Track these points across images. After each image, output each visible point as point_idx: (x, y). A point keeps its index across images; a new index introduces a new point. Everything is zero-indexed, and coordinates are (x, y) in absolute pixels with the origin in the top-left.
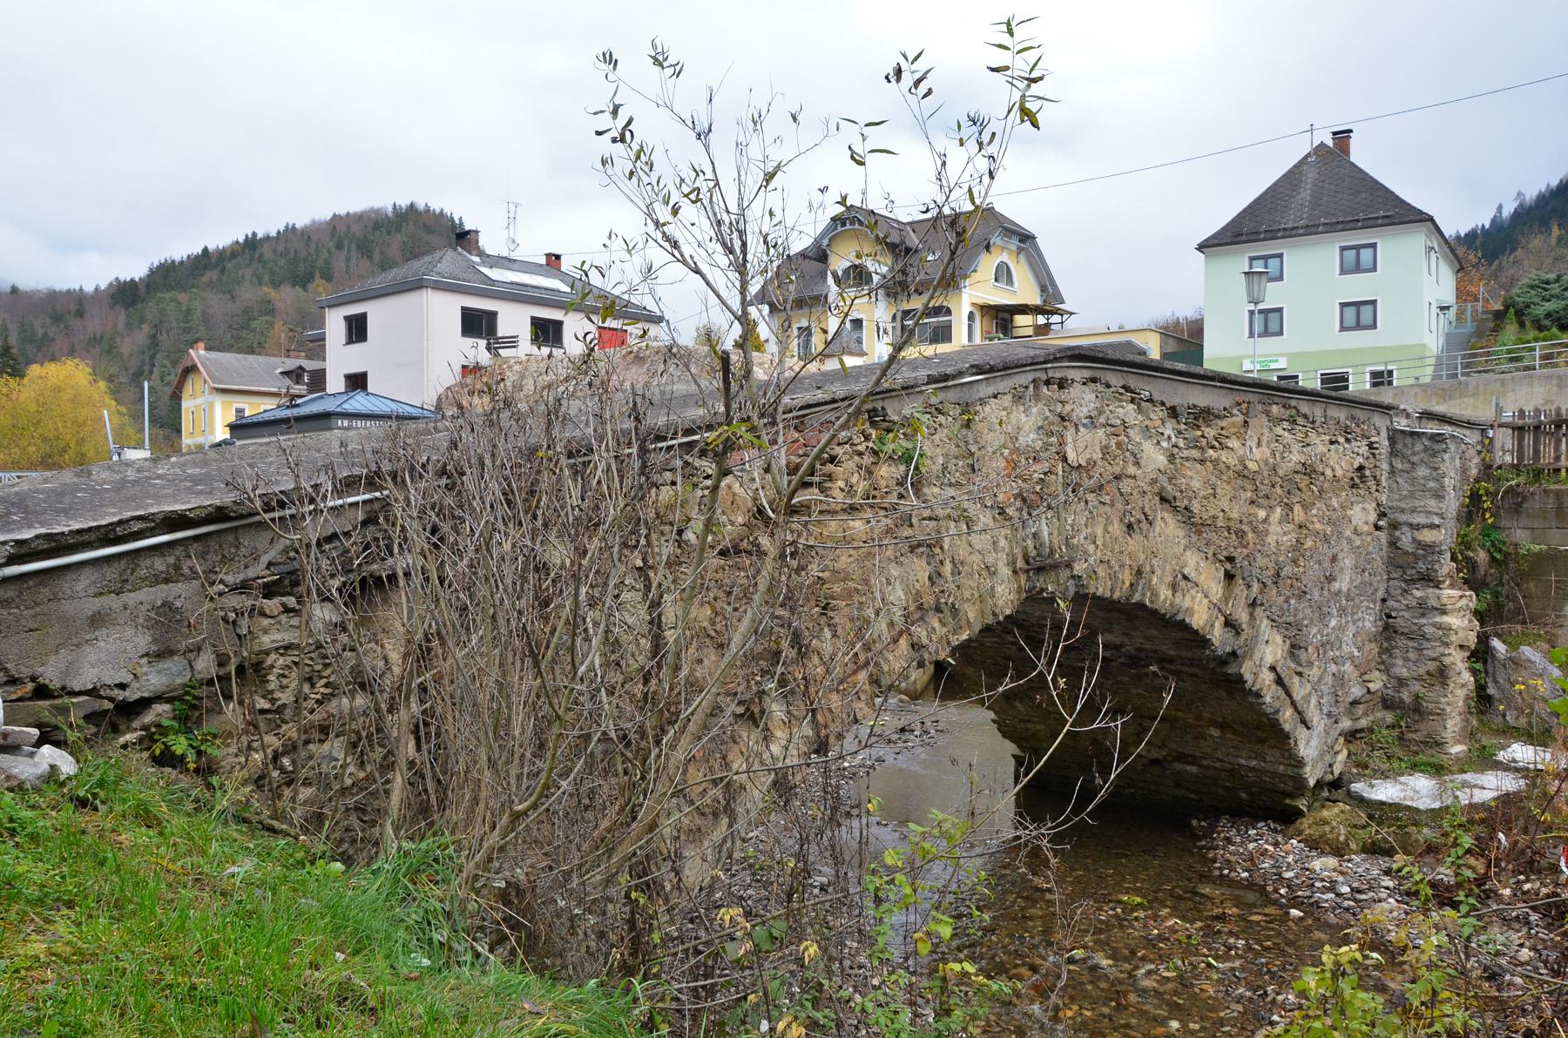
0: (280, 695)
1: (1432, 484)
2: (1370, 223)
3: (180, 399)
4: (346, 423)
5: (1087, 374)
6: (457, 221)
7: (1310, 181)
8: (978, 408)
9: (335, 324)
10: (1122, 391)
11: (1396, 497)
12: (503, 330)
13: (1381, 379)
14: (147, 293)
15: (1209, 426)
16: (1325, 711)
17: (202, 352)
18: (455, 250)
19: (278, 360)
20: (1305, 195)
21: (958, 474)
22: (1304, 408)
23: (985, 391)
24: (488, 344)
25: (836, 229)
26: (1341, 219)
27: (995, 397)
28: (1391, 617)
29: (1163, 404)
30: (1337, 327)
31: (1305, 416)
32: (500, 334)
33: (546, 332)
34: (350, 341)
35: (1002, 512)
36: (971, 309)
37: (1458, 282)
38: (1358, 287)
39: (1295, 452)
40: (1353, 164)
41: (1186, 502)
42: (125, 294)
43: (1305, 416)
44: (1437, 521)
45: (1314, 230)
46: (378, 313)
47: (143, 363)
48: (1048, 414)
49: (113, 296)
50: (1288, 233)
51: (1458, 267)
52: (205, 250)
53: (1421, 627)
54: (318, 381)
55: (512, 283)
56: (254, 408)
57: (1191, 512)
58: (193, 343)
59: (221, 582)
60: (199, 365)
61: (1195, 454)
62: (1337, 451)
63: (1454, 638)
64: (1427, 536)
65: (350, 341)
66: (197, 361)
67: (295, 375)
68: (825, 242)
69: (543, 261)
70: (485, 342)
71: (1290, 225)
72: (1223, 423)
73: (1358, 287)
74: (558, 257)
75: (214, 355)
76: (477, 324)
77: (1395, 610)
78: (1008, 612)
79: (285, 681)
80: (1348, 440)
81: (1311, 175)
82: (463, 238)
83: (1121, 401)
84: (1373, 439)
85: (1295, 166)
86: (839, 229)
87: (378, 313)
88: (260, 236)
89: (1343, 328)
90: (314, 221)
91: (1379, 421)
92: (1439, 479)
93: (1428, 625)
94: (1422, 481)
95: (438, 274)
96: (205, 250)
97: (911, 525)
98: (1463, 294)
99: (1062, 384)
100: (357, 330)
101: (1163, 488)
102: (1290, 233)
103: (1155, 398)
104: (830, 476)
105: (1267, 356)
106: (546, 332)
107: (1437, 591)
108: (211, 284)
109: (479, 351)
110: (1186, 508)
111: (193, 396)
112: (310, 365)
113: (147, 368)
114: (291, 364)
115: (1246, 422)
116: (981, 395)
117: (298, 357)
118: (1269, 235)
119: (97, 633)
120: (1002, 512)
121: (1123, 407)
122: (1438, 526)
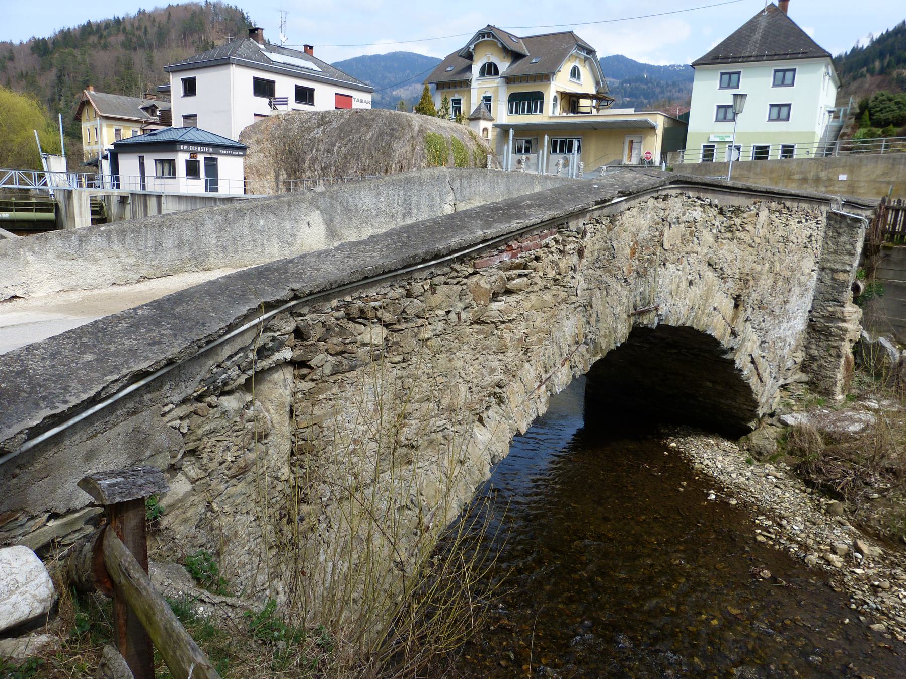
0: (210, 465)
1: (848, 247)
2: (795, 56)
3: (80, 121)
4: (185, 148)
5: (679, 191)
6: (245, 15)
7: (762, 27)
8: (619, 218)
9: (176, 84)
10: (696, 200)
11: (826, 252)
12: (278, 93)
13: (788, 151)
14: (54, 48)
15: (737, 217)
16: (773, 376)
17: (92, 92)
18: (249, 40)
19: (140, 100)
20: (758, 36)
21: (604, 261)
22: (788, 204)
23: (625, 206)
24: (270, 102)
25: (479, 39)
26: (778, 53)
27: (628, 209)
28: (813, 321)
29: (716, 206)
30: (767, 119)
31: (788, 208)
32: (276, 96)
33: (304, 95)
34: (186, 95)
35: (626, 281)
36: (555, 94)
37: (838, 93)
38: (782, 95)
39: (780, 230)
40: (789, 18)
41: (721, 265)
42: (40, 47)
43: (788, 208)
44: (848, 268)
45: (761, 58)
46: (202, 79)
47: (54, 93)
48: (656, 218)
49: (33, 49)
50: (745, 59)
51: (839, 84)
52: (89, 22)
53: (829, 328)
54: (166, 117)
55: (284, 64)
56: (127, 134)
57: (723, 271)
58: (87, 86)
59: (171, 402)
60: (91, 101)
61: (729, 235)
62: (800, 228)
63: (847, 336)
64: (841, 277)
65: (186, 95)
66: (89, 98)
67: (151, 109)
68: (472, 47)
69: (302, 49)
70: (267, 100)
71: (747, 54)
72: (745, 215)
73: (782, 95)
74: (311, 48)
75: (101, 95)
76: (263, 88)
77: (815, 317)
78: (623, 341)
79: (212, 455)
80: (807, 220)
81: (763, 23)
82: (254, 32)
83: (694, 206)
84: (819, 219)
85: (755, 18)
86: (481, 40)
87: (202, 79)
88: (121, 18)
89: (770, 120)
90: (156, 8)
91: (824, 209)
92: (853, 245)
93: (833, 327)
94: (843, 244)
95: (240, 56)
96: (89, 22)
97: (577, 295)
98: (840, 99)
99: (665, 198)
100: (190, 88)
101: (710, 258)
102: (747, 59)
103: (713, 203)
104: (534, 269)
105: (725, 133)
106: (304, 95)
107: (842, 309)
108: (94, 46)
109: (262, 104)
110: (721, 269)
111: (88, 120)
112: (161, 105)
113: (57, 97)
114: (148, 103)
115: (757, 214)
116: (622, 209)
117: (152, 99)
118: (734, 60)
119: (90, 465)
120: (626, 281)
121: (696, 210)
122: (848, 271)
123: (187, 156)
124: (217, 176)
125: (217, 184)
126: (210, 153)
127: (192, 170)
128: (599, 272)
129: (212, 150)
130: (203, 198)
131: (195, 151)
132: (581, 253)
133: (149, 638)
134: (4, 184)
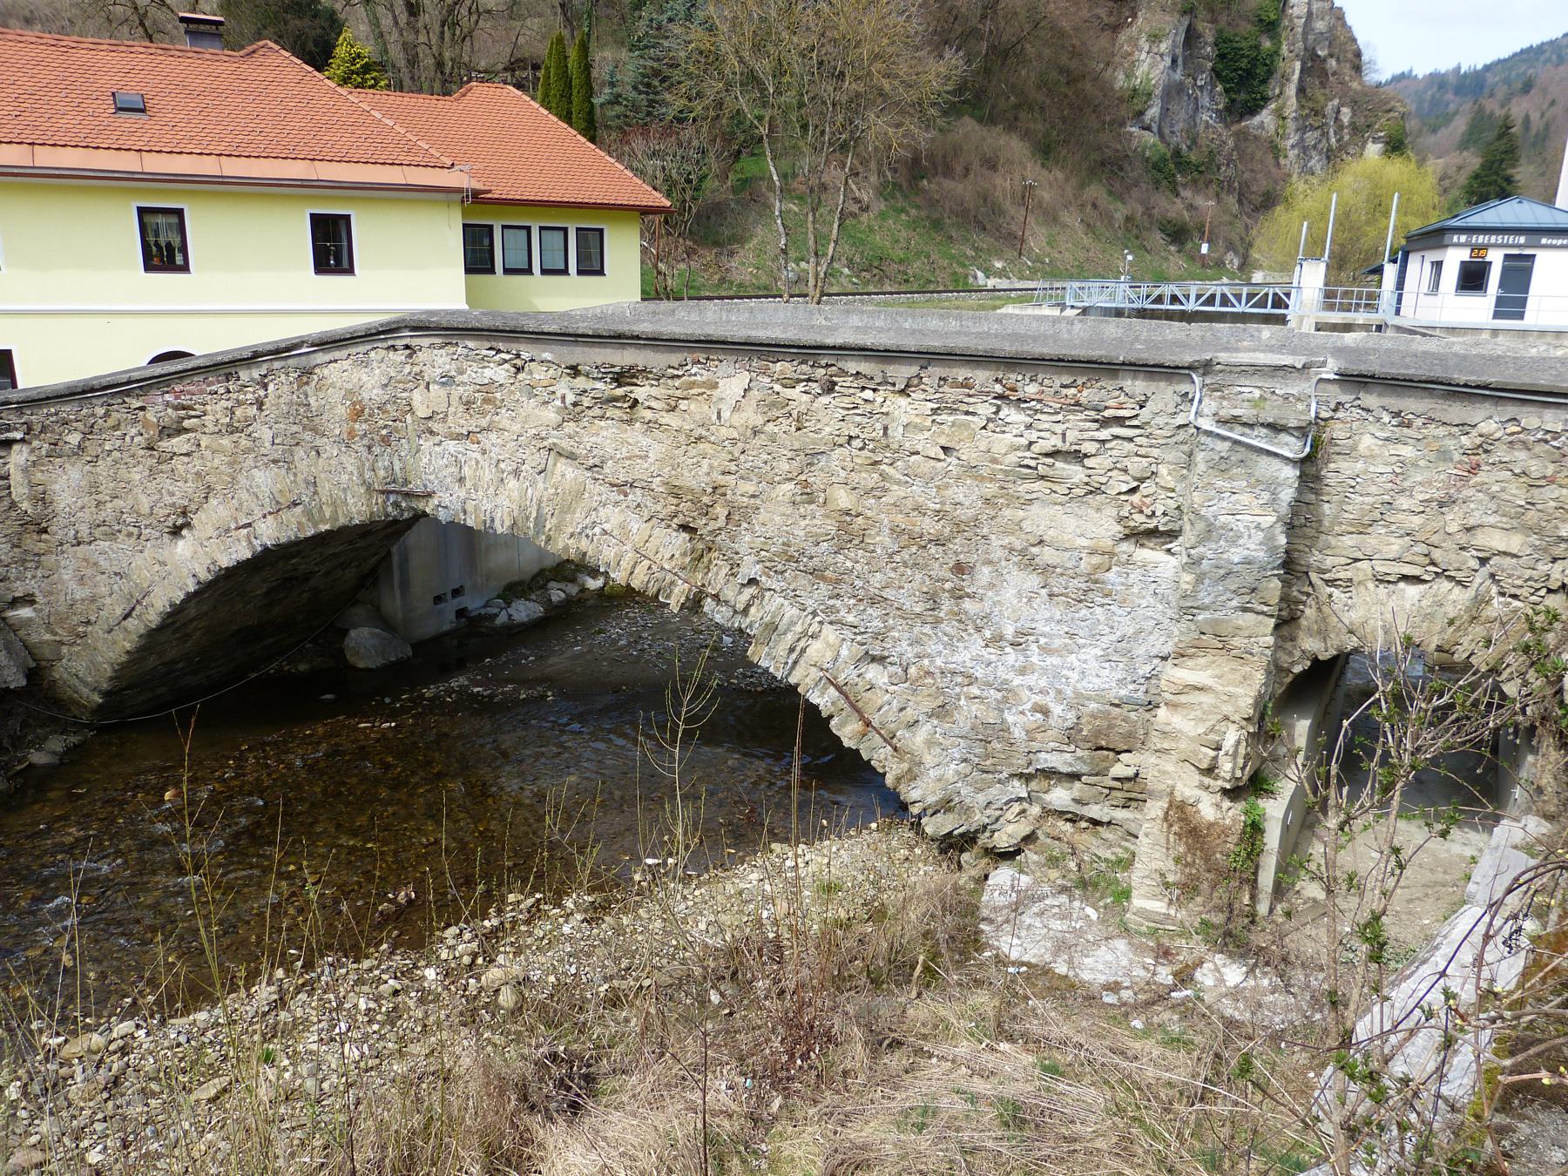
4: (1463, 238)
123: (1465, 255)
124: (1527, 292)
125: (1524, 306)
126: (1519, 246)
127: (1473, 278)
128: (295, 428)
129: (1522, 240)
130: (448, 330)
131: (1483, 244)
132: (260, 404)
133: (160, 629)
134: (1201, 305)
